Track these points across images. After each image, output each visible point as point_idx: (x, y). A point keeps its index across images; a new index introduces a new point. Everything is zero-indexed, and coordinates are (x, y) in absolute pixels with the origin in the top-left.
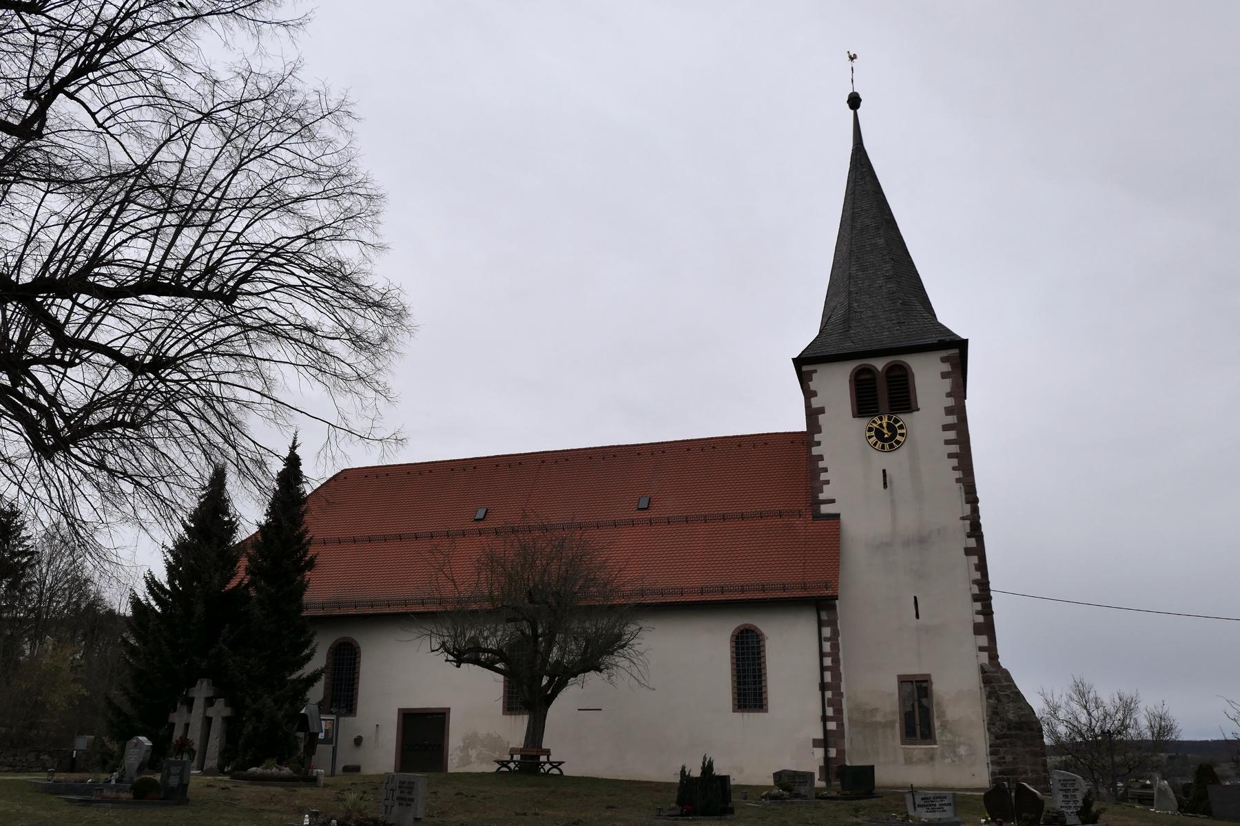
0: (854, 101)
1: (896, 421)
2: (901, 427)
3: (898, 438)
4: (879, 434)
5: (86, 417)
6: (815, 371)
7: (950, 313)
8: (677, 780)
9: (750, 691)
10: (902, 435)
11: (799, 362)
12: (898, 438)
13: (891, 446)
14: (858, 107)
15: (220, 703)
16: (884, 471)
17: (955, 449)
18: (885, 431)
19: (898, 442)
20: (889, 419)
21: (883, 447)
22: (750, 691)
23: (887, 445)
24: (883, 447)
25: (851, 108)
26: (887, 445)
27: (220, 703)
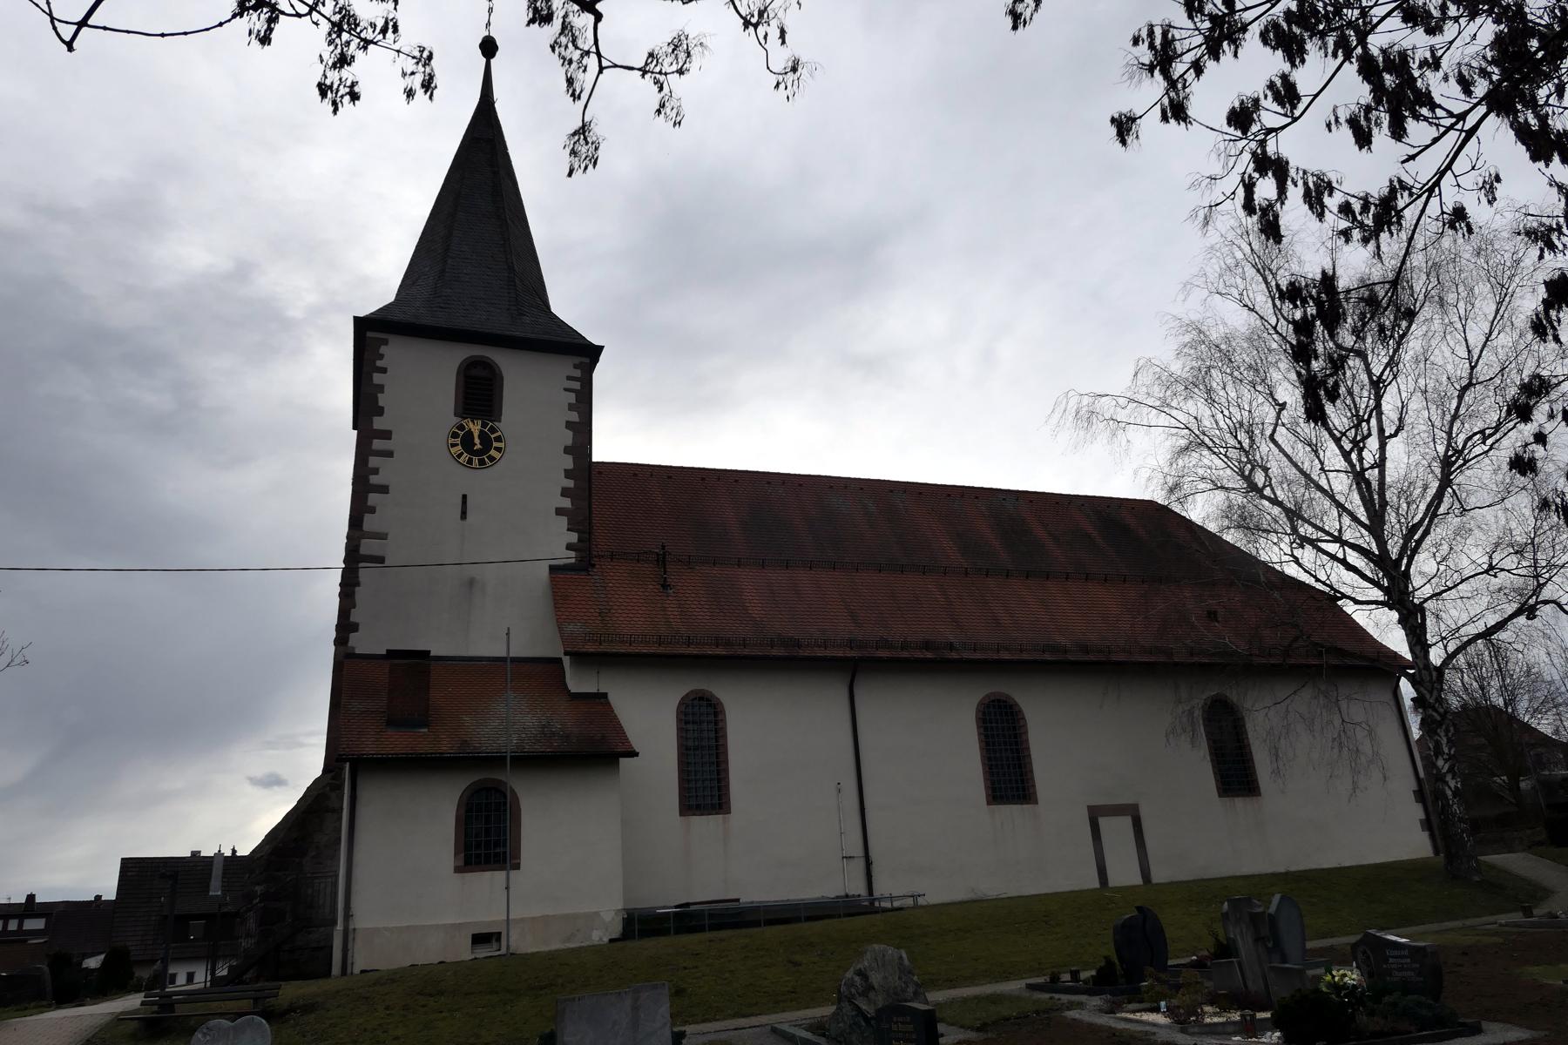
0: (489, 47)
1: (493, 430)
2: (498, 439)
3: (493, 452)
4: (467, 441)
5: (1069, 1009)
6: (385, 342)
7: (568, 300)
8: (1318, 277)
9: (1009, 778)
10: (498, 450)
11: (363, 326)
12: (493, 452)
13: (482, 462)
14: (493, 55)
15: (1058, 728)
16: (464, 497)
17: (577, 385)
18: (477, 441)
19: (492, 459)
20: (484, 425)
21: (470, 461)
22: (1009, 778)
23: (476, 460)
24: (470, 461)
25: (484, 54)
26: (476, 460)
27: (1058, 728)
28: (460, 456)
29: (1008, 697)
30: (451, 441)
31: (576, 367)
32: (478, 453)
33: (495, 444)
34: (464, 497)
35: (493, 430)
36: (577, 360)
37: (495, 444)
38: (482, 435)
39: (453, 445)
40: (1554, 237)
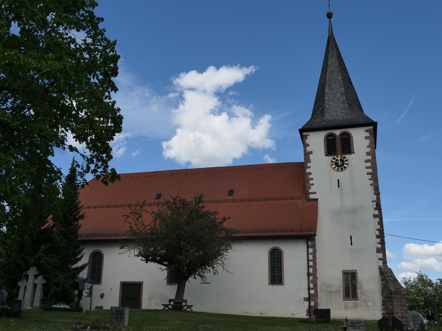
1: (344, 158)
2: (346, 161)
3: (345, 165)
4: (337, 164)
6: (309, 135)
9: (276, 276)
10: (347, 164)
12: (345, 165)
13: (342, 169)
15: (40, 278)
19: (345, 167)
20: (341, 157)
21: (338, 169)
22: (276, 276)
23: (340, 168)
24: (338, 169)
28: (335, 168)
29: (279, 248)
30: (347, 162)
31: (366, 131)
32: (340, 166)
33: (345, 162)
34: (338, 180)
35: (344, 158)
36: (367, 128)
37: (345, 162)
38: (341, 160)
39: (332, 165)
40: (23, 4)
